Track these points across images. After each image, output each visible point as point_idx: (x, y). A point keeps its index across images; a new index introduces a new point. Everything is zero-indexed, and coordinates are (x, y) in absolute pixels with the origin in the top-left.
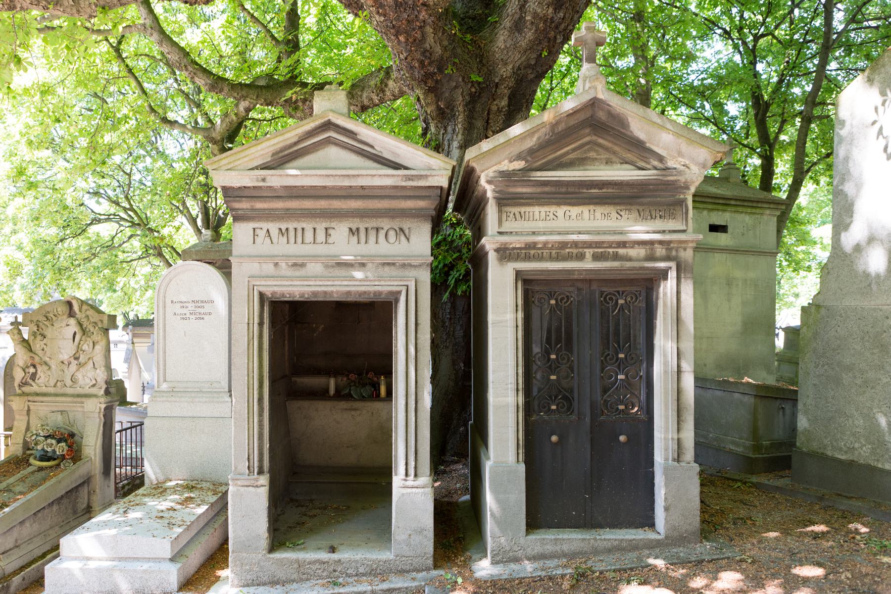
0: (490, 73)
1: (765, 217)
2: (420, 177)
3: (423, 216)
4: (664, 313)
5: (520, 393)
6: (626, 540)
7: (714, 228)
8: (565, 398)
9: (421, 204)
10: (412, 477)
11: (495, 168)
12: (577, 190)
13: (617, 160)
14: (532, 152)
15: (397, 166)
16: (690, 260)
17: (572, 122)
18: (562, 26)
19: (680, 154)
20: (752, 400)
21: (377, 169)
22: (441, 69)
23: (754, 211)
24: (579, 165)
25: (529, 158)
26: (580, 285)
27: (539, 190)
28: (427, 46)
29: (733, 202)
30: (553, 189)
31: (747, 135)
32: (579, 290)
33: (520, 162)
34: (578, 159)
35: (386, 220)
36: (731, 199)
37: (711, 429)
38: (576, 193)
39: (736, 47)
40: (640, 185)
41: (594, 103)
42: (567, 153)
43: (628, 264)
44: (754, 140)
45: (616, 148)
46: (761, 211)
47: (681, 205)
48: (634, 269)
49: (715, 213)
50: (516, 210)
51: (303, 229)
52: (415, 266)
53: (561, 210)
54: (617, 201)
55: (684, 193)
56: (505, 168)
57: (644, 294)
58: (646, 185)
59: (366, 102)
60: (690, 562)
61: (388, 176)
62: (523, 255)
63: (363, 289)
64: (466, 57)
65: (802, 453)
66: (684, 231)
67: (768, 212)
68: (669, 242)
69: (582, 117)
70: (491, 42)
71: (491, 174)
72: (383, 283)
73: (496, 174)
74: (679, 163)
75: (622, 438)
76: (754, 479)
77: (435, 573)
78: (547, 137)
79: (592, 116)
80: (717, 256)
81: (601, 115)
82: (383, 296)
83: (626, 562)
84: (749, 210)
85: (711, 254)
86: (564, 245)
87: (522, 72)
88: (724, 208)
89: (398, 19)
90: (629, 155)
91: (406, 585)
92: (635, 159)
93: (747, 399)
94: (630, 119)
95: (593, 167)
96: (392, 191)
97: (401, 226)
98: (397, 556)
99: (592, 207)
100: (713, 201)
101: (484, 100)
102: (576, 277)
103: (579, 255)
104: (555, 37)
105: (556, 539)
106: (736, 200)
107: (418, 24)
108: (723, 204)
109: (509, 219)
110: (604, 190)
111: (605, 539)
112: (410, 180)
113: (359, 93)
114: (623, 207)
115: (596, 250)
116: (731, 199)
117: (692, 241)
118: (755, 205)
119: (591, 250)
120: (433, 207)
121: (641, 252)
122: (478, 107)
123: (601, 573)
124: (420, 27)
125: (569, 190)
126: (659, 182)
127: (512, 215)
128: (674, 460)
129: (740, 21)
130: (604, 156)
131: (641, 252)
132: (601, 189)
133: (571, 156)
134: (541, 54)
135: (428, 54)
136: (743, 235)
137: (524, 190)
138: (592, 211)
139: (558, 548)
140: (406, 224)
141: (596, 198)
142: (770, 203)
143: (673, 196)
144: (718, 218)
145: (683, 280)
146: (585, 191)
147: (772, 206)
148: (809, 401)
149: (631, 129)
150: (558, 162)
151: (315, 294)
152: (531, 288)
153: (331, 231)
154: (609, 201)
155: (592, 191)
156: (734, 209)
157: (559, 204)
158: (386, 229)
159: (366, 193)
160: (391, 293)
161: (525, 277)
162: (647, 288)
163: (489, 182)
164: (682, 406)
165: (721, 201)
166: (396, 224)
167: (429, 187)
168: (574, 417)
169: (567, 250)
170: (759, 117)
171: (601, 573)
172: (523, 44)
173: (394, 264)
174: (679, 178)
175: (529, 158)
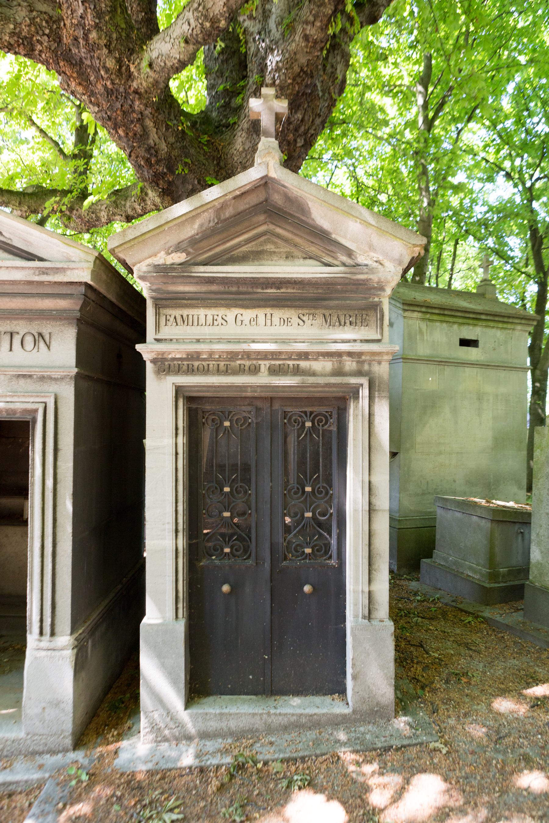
1: (517, 333)
2: (57, 270)
3: (66, 319)
4: (354, 440)
5: (180, 535)
6: (306, 715)
7: (464, 343)
8: (240, 539)
9: (63, 304)
10: (47, 637)
11: (149, 261)
12: (250, 290)
13: (300, 254)
14: (193, 242)
15: (29, 257)
16: (386, 376)
17: (242, 206)
18: (302, 129)
19: (371, 247)
20: (489, 525)
21: (9, 260)
22: (171, 169)
23: (505, 326)
24: (253, 260)
25: (191, 250)
26: (259, 404)
27: (204, 288)
28: (151, 142)
29: (483, 317)
30: (221, 288)
31: (527, 265)
32: (258, 410)
33: (179, 254)
34: (252, 252)
35: (21, 322)
36: (482, 314)
37: (451, 552)
38: (249, 293)
39: (516, 186)
40: (324, 284)
42: (239, 245)
43: (311, 380)
44: (531, 269)
45: (298, 240)
46: (512, 327)
47: (376, 310)
48: (317, 385)
49: (466, 327)
50: (177, 312)
52: (56, 380)
53: (231, 314)
54: (297, 303)
55: (378, 296)
56: (161, 262)
57: (335, 416)
58: (332, 284)
59: (130, 212)
60: (375, 749)
61: (17, 268)
62: (185, 368)
64: (202, 158)
65: (534, 588)
66: (379, 341)
67: (519, 327)
68: (360, 354)
69: (253, 200)
70: (229, 144)
71: (145, 269)
72: (15, 399)
73: (150, 269)
74: (371, 259)
75: (307, 588)
76: (487, 613)
77: (72, 756)
78: (211, 224)
79: (266, 200)
80: (469, 371)
81: (277, 199)
82: (18, 415)
83: (300, 746)
84: (500, 325)
85: (461, 369)
86: (233, 356)
88: (475, 322)
89: (111, 108)
90: (313, 249)
92: (319, 253)
93: (483, 523)
94: (310, 204)
95: (270, 262)
96: (26, 287)
97: (40, 331)
98: (28, 734)
99: (268, 311)
100: (463, 315)
102: (249, 394)
103: (253, 368)
104: (295, 141)
105: (221, 714)
106: (487, 314)
107: (135, 116)
108: (473, 319)
109: (169, 323)
110: (282, 291)
111: (280, 714)
112: (44, 273)
113: (123, 203)
114: (305, 311)
115: (273, 362)
116: (482, 314)
117: (387, 353)
118: (506, 320)
119: (267, 363)
120: (78, 308)
121: (326, 365)
123: (266, 763)
124: (138, 120)
125: (241, 289)
126: (347, 281)
127: (172, 319)
128: (364, 617)
129: (503, 148)
130: (285, 248)
131: (326, 365)
132: (279, 288)
133: (244, 249)
135: (153, 151)
136: (494, 349)
137: (187, 288)
138: (269, 316)
139: (224, 725)
140: (46, 328)
141: (274, 300)
142: (522, 319)
143: (366, 298)
144: (469, 333)
145: (377, 400)
146: (260, 290)
147: (523, 322)
148: (542, 532)
149: (313, 216)
150: (228, 256)
152: (196, 410)
154: (289, 303)
156: (484, 324)
157: (228, 306)
160: (26, 411)
161: (187, 394)
162: (339, 408)
163: (142, 278)
164: (374, 552)
165: (471, 316)
166: (35, 327)
167: (72, 283)
168: (250, 562)
169: (239, 362)
170: (536, 248)
171: (266, 763)
173: (30, 376)
174: (371, 276)
175: (191, 250)
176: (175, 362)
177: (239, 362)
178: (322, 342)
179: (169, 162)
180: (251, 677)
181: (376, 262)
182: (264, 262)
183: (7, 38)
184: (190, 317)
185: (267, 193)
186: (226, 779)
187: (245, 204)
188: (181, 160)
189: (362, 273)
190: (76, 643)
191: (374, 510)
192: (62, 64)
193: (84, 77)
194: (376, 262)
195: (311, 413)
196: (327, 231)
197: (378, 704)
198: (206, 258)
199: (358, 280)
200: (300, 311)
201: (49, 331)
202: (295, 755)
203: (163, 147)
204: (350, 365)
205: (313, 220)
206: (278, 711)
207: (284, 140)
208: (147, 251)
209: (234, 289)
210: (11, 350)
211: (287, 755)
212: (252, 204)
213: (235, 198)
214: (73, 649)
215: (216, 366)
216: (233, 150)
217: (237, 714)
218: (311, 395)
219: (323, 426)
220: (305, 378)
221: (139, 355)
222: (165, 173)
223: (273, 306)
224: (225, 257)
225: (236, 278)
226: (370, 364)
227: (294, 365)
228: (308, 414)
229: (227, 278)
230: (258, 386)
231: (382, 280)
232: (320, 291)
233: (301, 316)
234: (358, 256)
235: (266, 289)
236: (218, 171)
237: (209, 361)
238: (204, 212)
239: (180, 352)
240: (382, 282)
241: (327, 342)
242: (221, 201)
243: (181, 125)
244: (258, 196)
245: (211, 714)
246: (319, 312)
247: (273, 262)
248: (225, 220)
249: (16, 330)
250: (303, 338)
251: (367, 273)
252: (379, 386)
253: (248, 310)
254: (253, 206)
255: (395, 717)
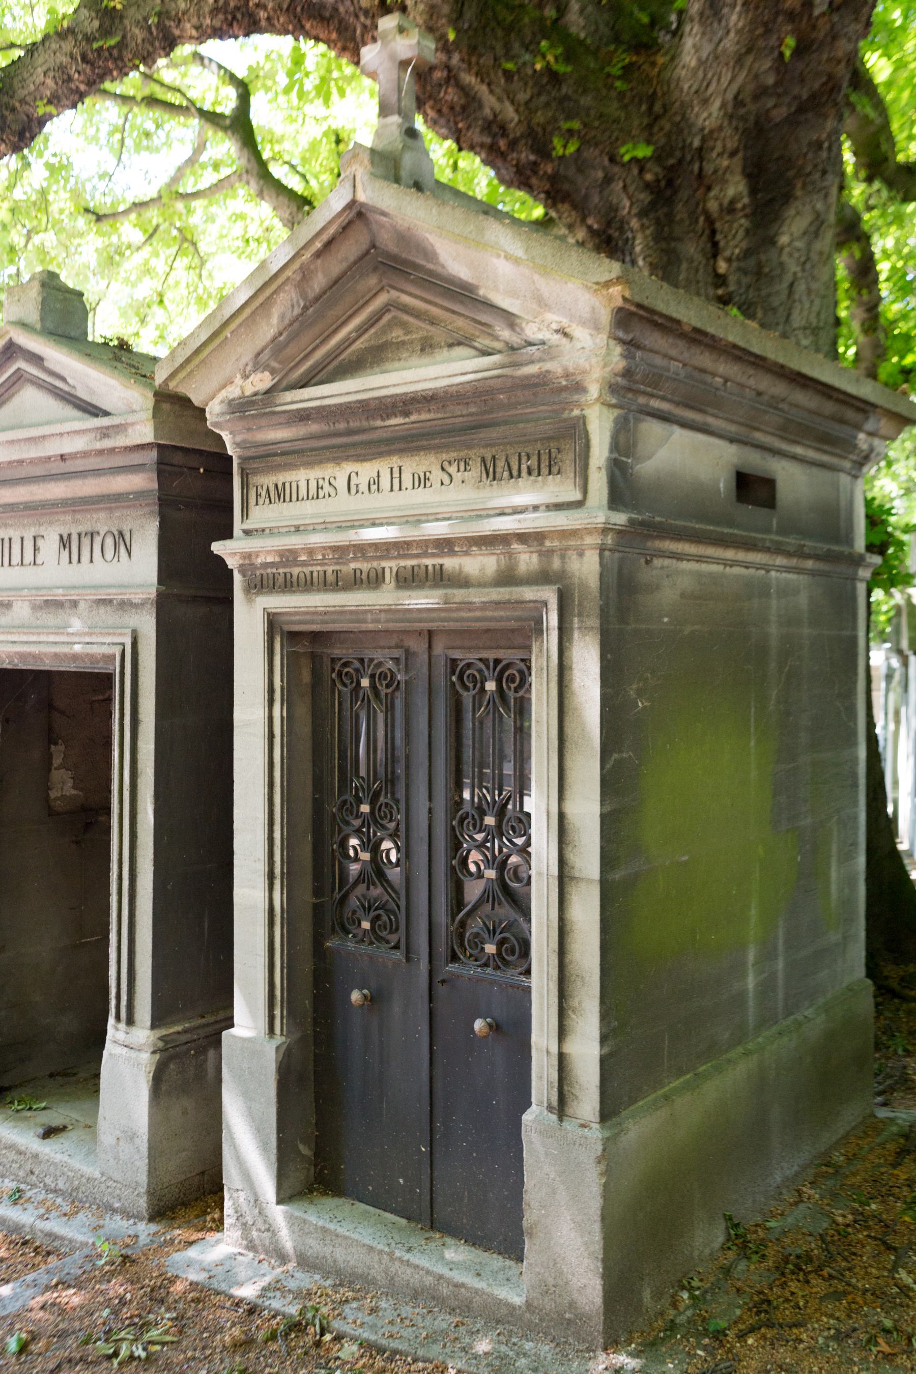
0: (682, 126)
6: (449, 1282)
12: (365, 424)
15: (94, 411)
17: (335, 265)
19: (542, 303)
21: (74, 419)
22: (543, 151)
25: (275, 364)
27: (300, 431)
41: (357, 215)
42: (348, 342)
43: (459, 595)
51: (10, 539)
53: (340, 473)
63: (34, 649)
66: (579, 504)
69: (350, 250)
70: (673, 59)
78: (297, 311)
81: (386, 241)
87: (752, 107)
91: (70, 1235)
95: (397, 365)
99: (395, 461)
101: (684, 194)
105: (324, 1230)
109: (261, 501)
110: (414, 418)
115: (403, 563)
122: (681, 211)
126: (509, 383)
127: (264, 493)
130: (423, 329)
132: (407, 414)
133: (358, 345)
134: (781, 55)
135: (495, 129)
138: (396, 470)
145: (576, 635)
146: (379, 423)
151: (22, 656)
153: (40, 542)
155: (393, 421)
157: (337, 460)
158: (102, 533)
159: (70, 466)
161: (287, 628)
164: (572, 969)
169: (353, 565)
172: (730, 43)
173: (111, 601)
174: (548, 366)
175: (275, 364)
176: (269, 571)
177: (353, 565)
178: (482, 515)
179: (534, 140)
180: (401, 1181)
181: (557, 331)
182: (388, 366)
183: (208, 21)
184: (287, 486)
185: (370, 230)
186: (261, 1336)
187: (341, 262)
188: (559, 128)
189: (532, 362)
190: (161, 1044)
191: (572, 878)
192: (308, 26)
193: (349, 34)
194: (557, 331)
195: (497, 662)
196: (470, 284)
197: (572, 1305)
198: (302, 375)
199: (527, 377)
200: (444, 456)
201: (130, 527)
202: (384, 1342)
203: (510, 113)
204: (527, 560)
205: (443, 267)
206: (407, 1256)
207: (777, 13)
208: (215, 380)
209: (342, 426)
210: (91, 561)
211: (373, 1338)
212: (352, 259)
213: (318, 254)
214: (154, 1052)
215: (322, 573)
216: (678, 70)
217: (346, 1238)
218: (465, 625)
219: (516, 691)
220: (450, 591)
221: (220, 561)
222: (535, 163)
223: (401, 452)
224: (331, 367)
225: (335, 405)
226: (563, 557)
227: (434, 566)
228: (491, 664)
229: (323, 408)
230: (380, 611)
231: (571, 370)
232: (473, 409)
233: (446, 464)
234: (524, 325)
235: (388, 417)
236: (650, 126)
237: (312, 565)
238: (275, 292)
239: (269, 552)
240: (573, 374)
241: (488, 516)
242: (296, 266)
243: (539, 58)
244: (357, 241)
245: (311, 1223)
246: (475, 454)
247: (402, 363)
248: (317, 299)
249: (96, 529)
250: (445, 509)
251: (540, 360)
252: (580, 604)
253: (365, 464)
254: (355, 263)
255: (605, 1349)
